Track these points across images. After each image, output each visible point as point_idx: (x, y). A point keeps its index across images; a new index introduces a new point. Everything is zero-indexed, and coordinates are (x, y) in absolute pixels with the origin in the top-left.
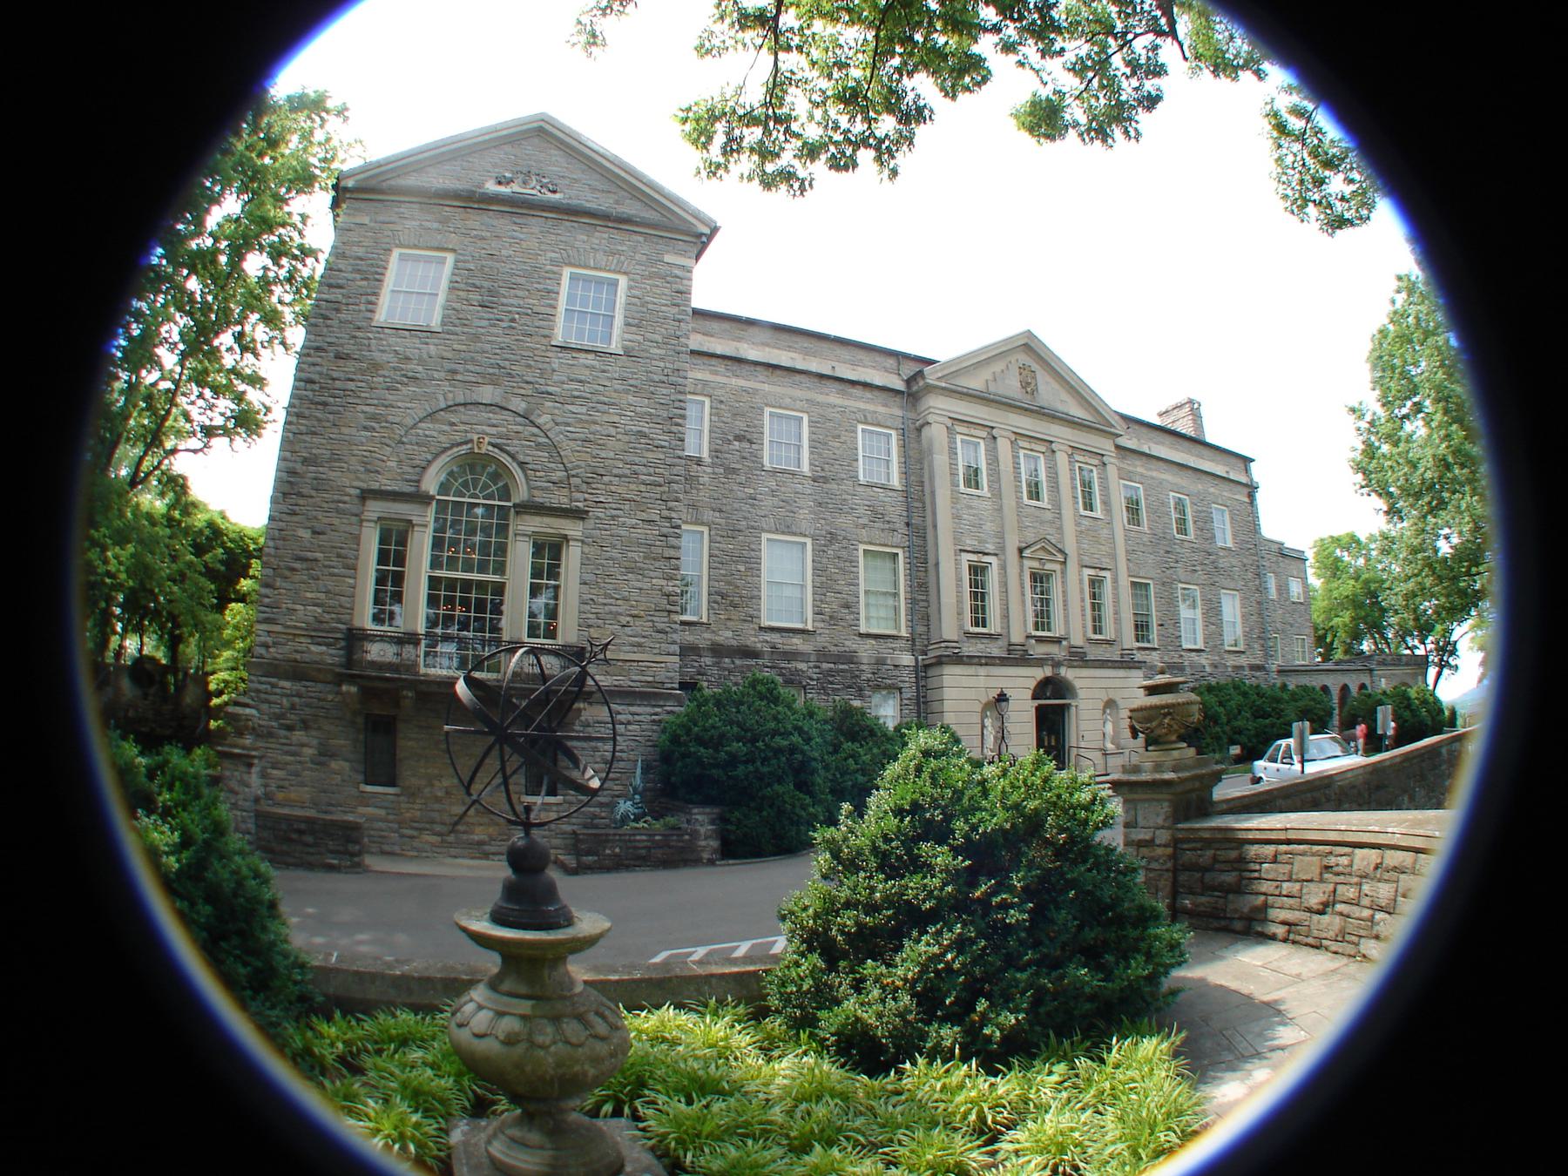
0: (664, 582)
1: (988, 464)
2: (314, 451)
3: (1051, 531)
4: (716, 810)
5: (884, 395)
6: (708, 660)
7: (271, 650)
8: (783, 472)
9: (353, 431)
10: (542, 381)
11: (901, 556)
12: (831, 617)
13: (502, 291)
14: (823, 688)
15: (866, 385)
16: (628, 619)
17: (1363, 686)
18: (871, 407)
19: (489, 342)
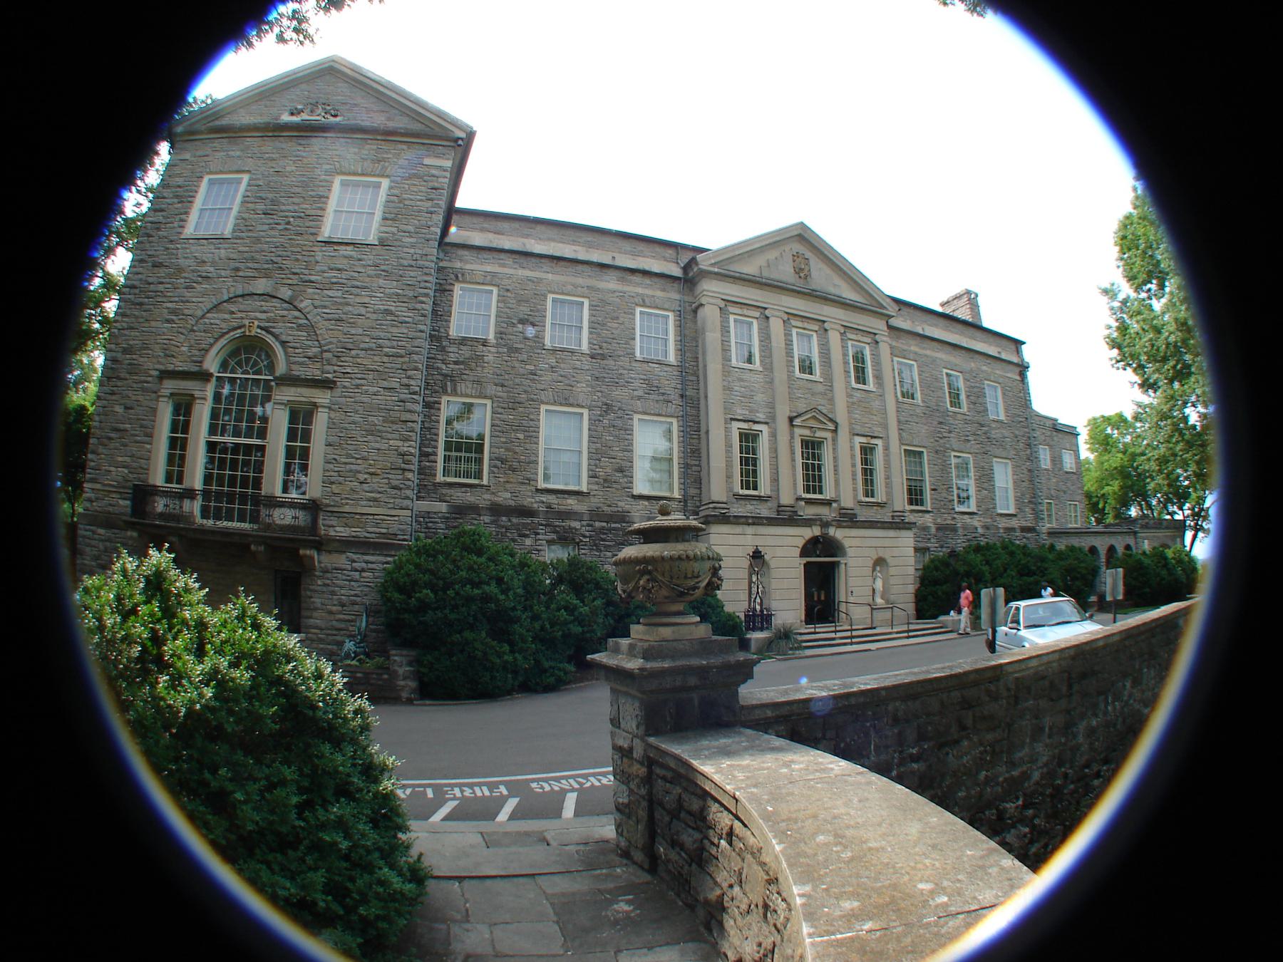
0: (400, 443)
1: (761, 341)
2: (131, 342)
3: (823, 402)
4: (413, 653)
5: (662, 281)
6: (487, 519)
7: (94, 504)
8: (563, 350)
9: (158, 324)
10: (306, 272)
11: (925, 454)
12: (605, 481)
13: (282, 200)
14: (595, 545)
15: (645, 273)
16: (366, 476)
17: (1128, 547)
18: (649, 292)
19: (267, 243)
